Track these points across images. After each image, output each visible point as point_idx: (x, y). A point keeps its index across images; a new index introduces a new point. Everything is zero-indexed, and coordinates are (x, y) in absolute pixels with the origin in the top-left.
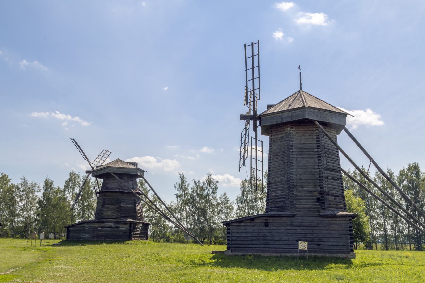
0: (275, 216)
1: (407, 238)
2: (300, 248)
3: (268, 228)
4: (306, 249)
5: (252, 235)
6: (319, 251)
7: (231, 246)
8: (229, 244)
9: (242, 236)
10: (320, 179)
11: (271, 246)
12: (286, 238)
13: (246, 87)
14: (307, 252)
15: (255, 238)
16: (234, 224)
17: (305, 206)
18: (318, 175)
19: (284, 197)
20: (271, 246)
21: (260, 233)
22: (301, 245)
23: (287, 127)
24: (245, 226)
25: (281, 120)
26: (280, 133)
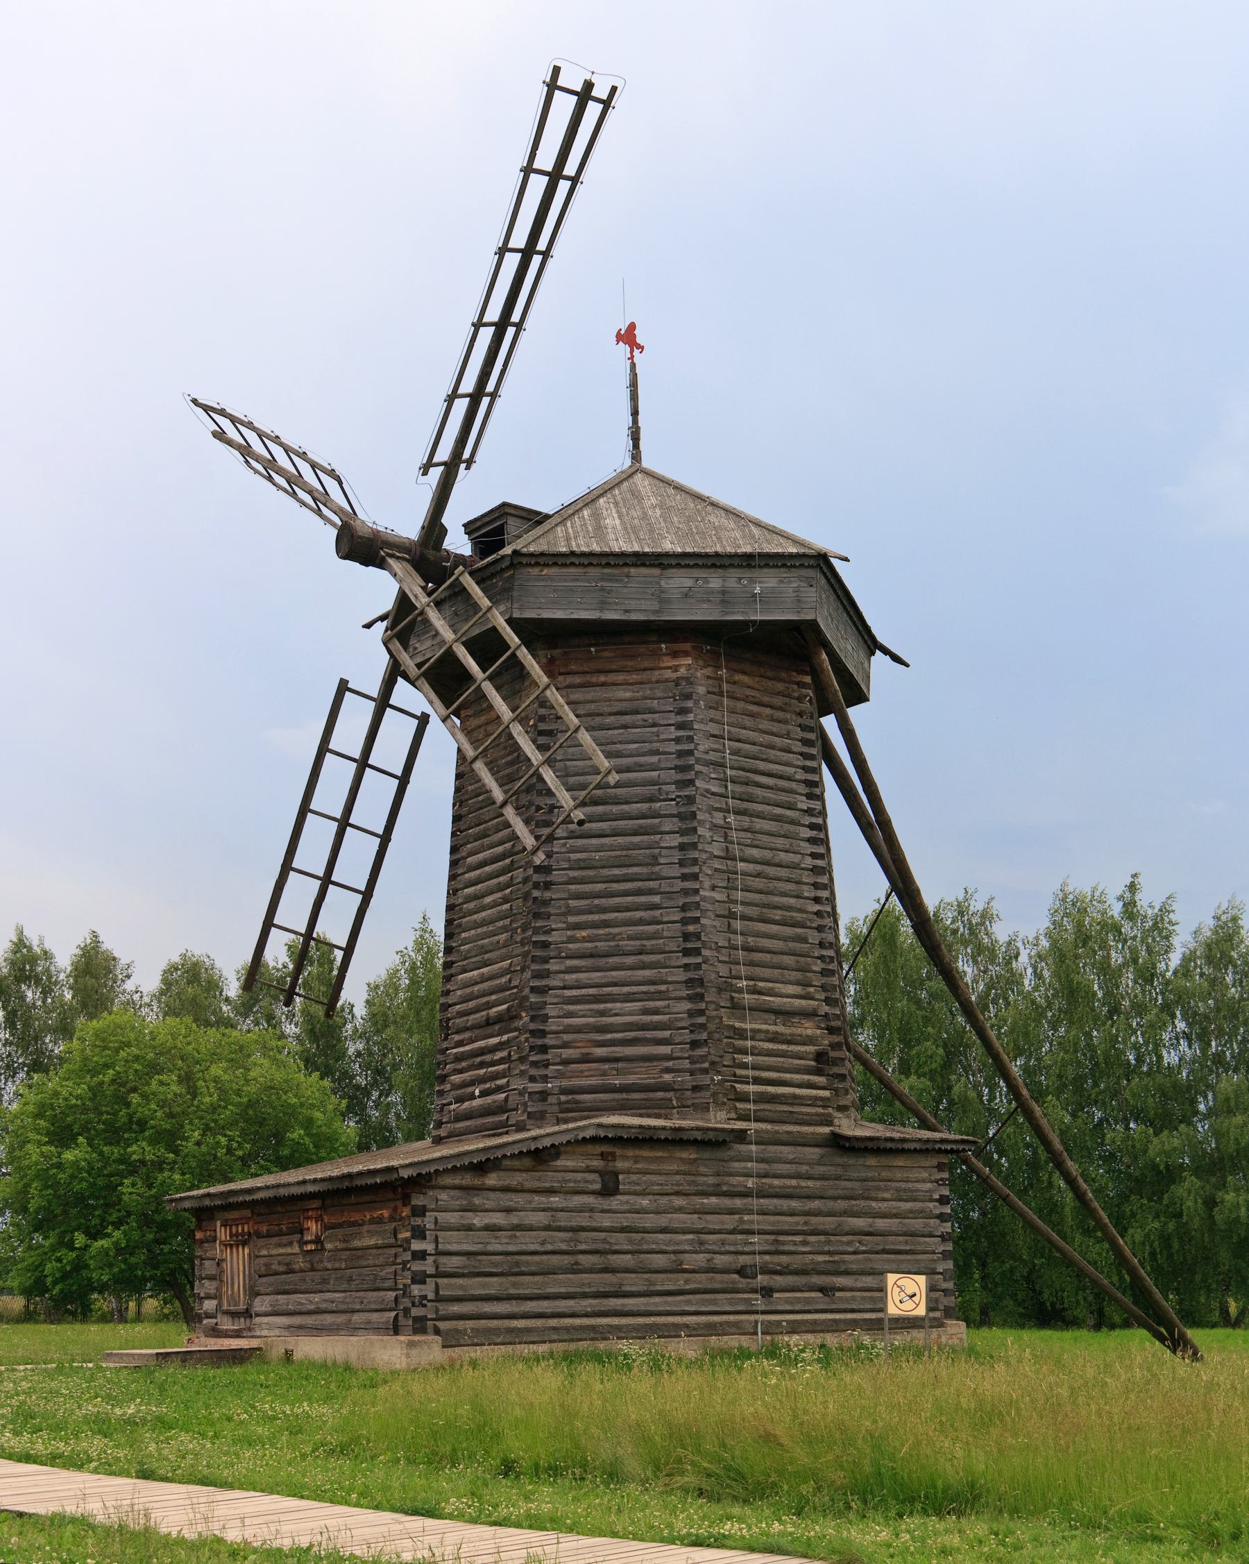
0: (659, 1140)
1: (1114, 937)
2: (892, 1310)
3: (615, 1202)
4: (921, 1311)
5: (652, 1283)
6: (832, 1320)
7: (437, 1311)
8: (425, 1297)
9: (490, 1248)
10: (824, 952)
11: (631, 1303)
12: (700, 1259)
13: (546, 88)
14: (886, 1322)
15: (555, 1260)
16: (448, 1180)
17: (798, 1091)
18: (816, 933)
19: (667, 1034)
20: (631, 1303)
21: (583, 1229)
22: (896, 1290)
23: (675, 654)
24: (506, 1190)
25: (655, 606)
26: (620, 677)
